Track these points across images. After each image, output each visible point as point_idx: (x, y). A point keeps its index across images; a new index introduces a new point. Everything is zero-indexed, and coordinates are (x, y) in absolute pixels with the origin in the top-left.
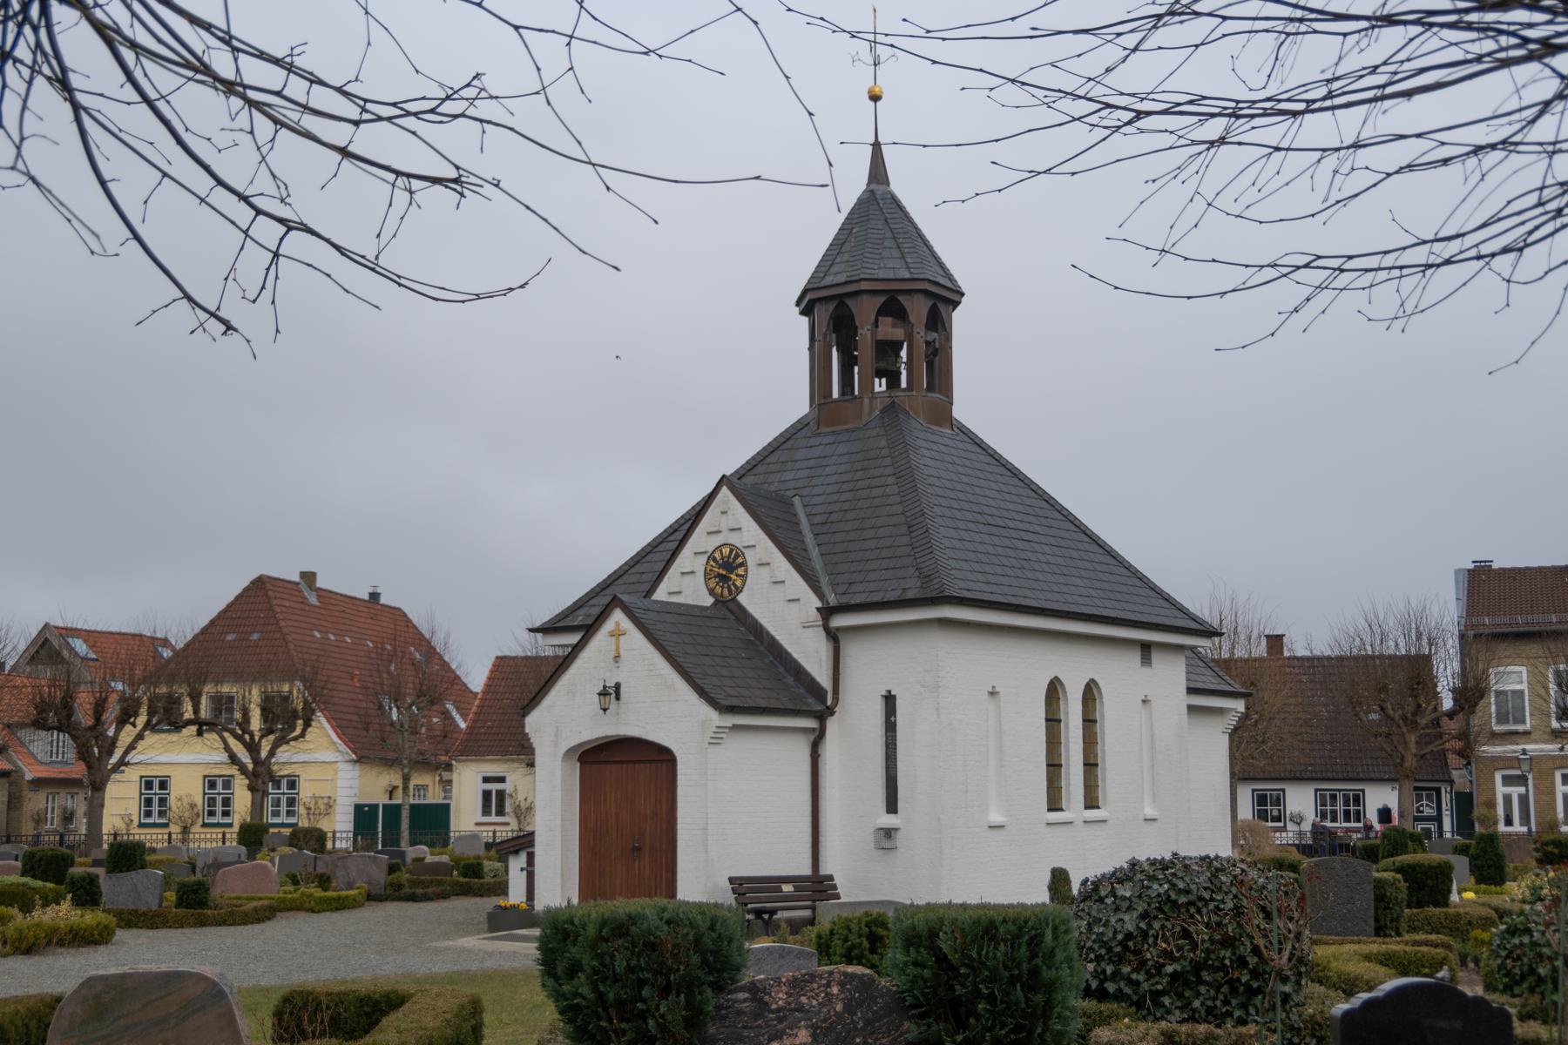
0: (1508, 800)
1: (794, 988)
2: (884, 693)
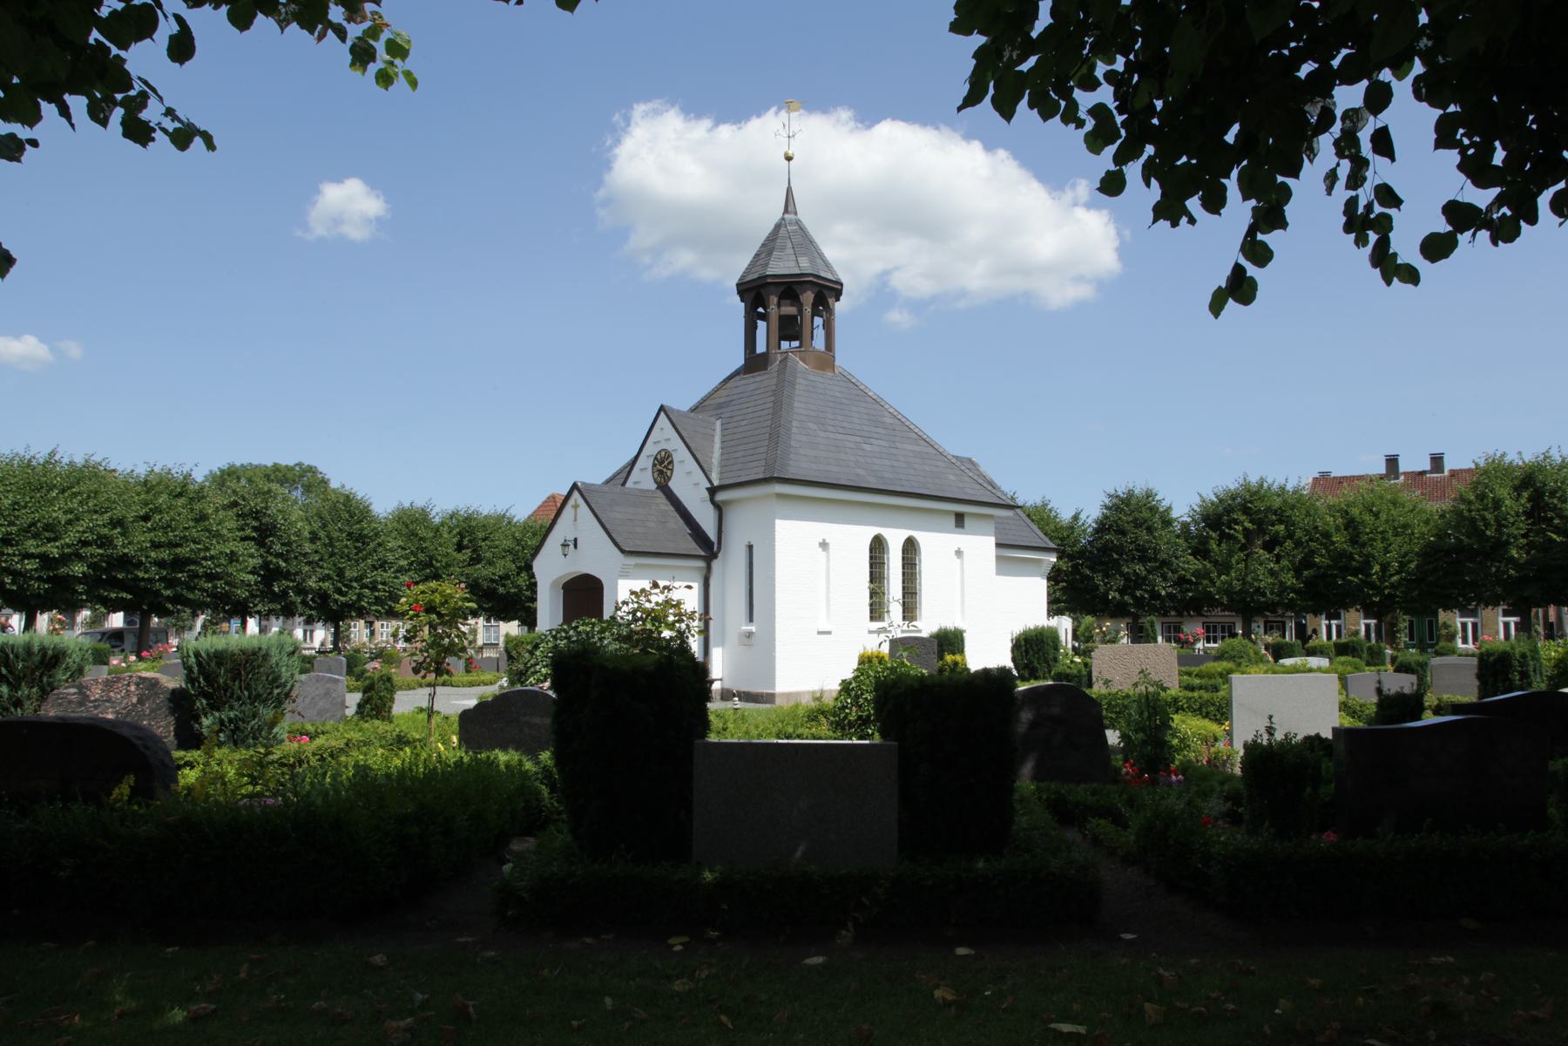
1: (106, 686)
2: (821, 541)
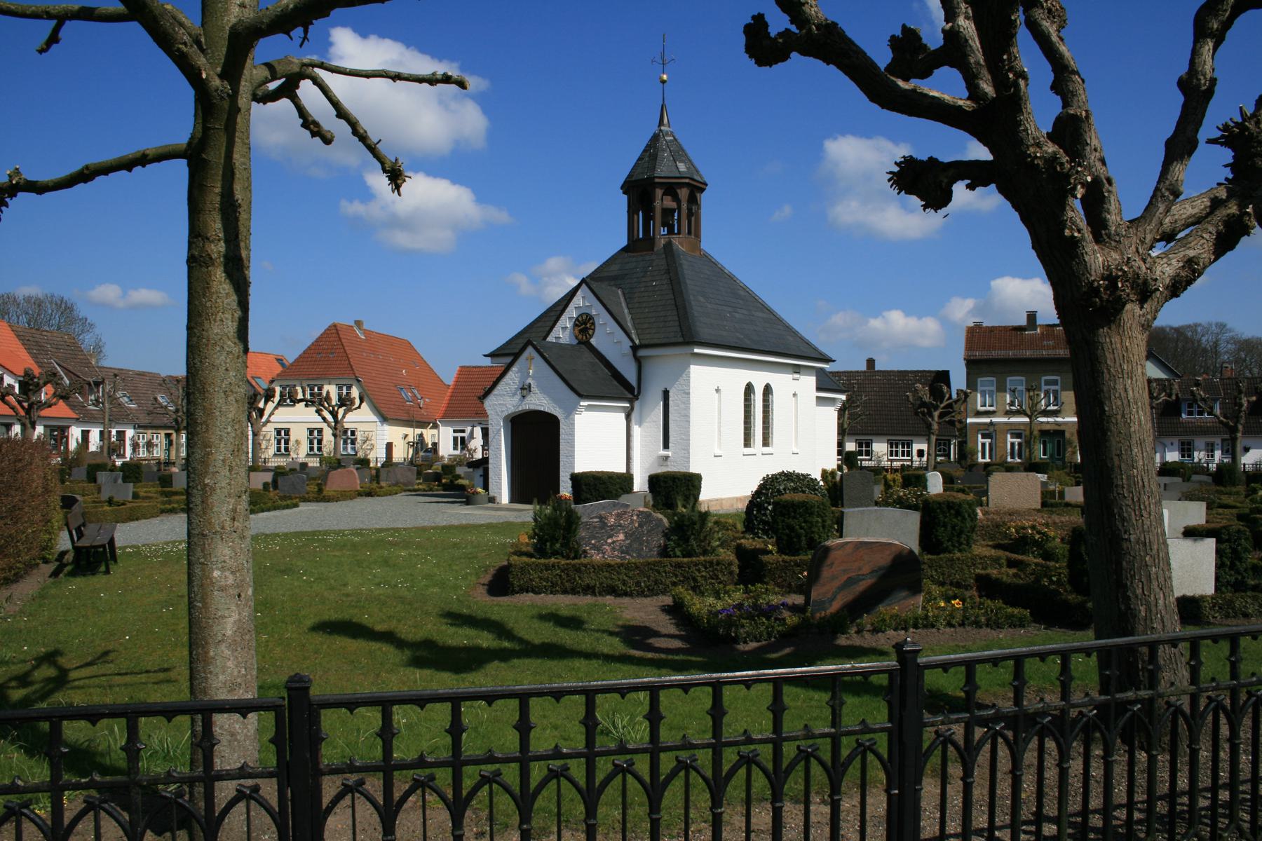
0: (983, 445)
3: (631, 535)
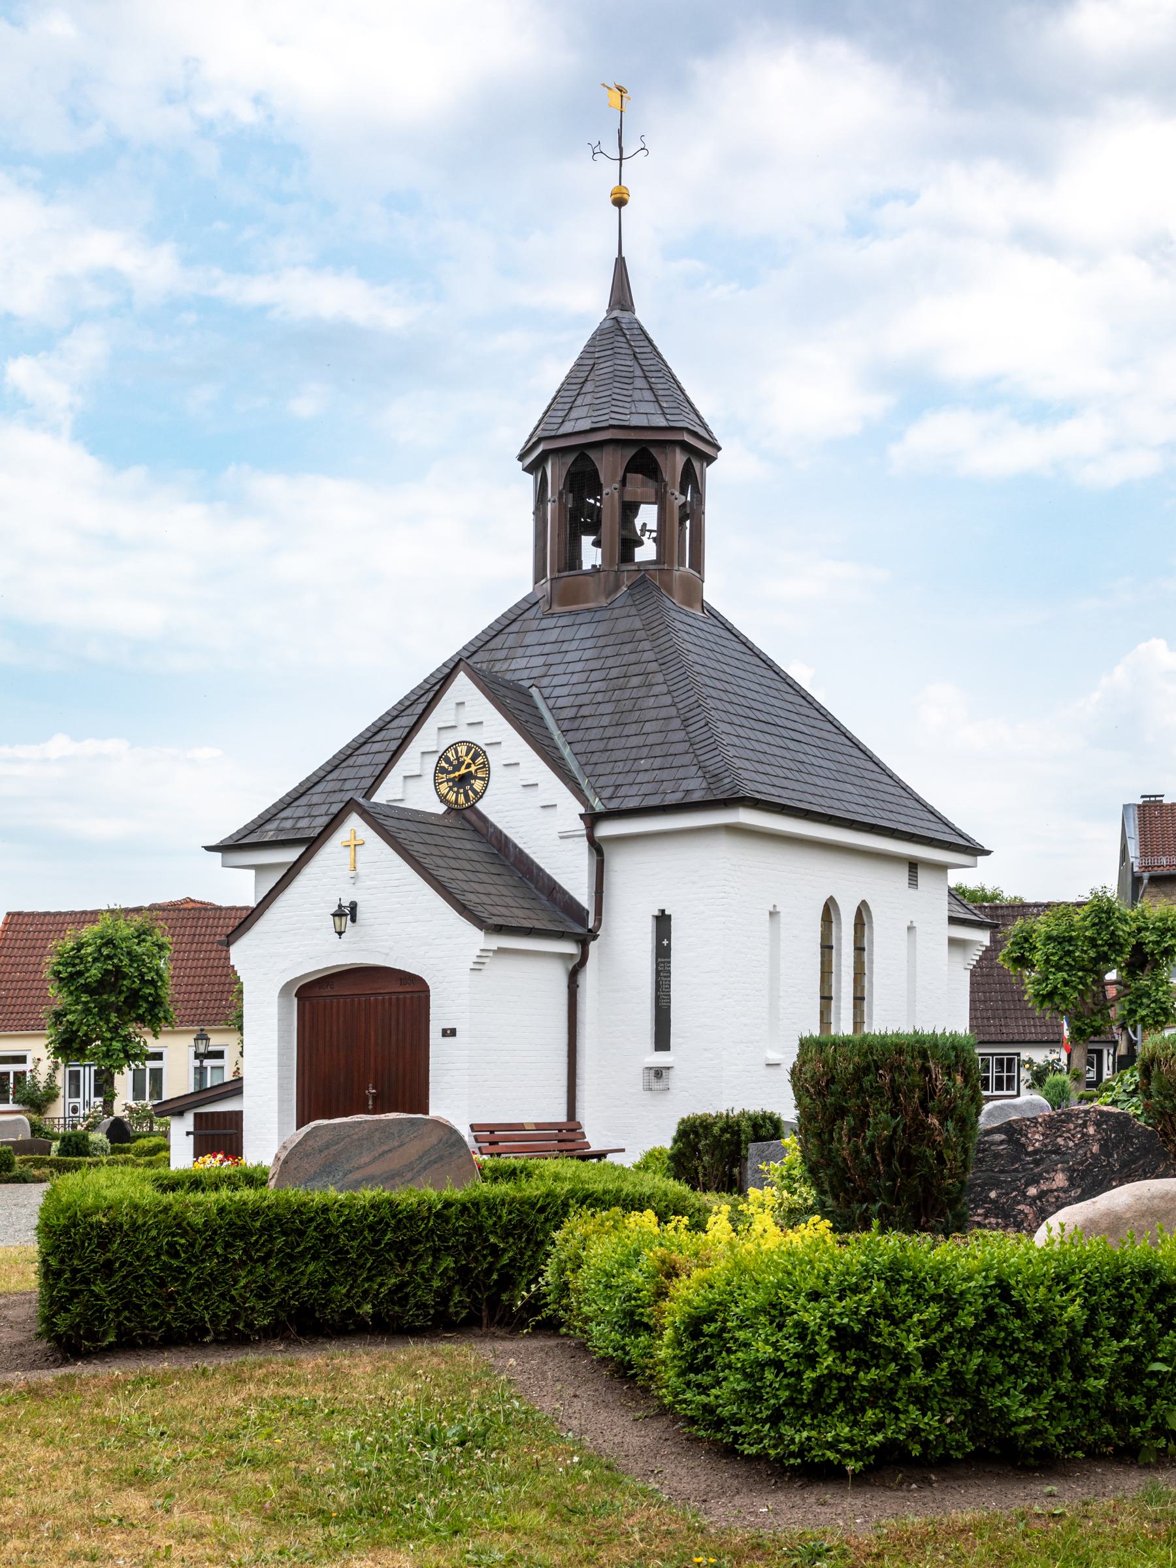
2: (657, 913)
3: (1084, 1175)
